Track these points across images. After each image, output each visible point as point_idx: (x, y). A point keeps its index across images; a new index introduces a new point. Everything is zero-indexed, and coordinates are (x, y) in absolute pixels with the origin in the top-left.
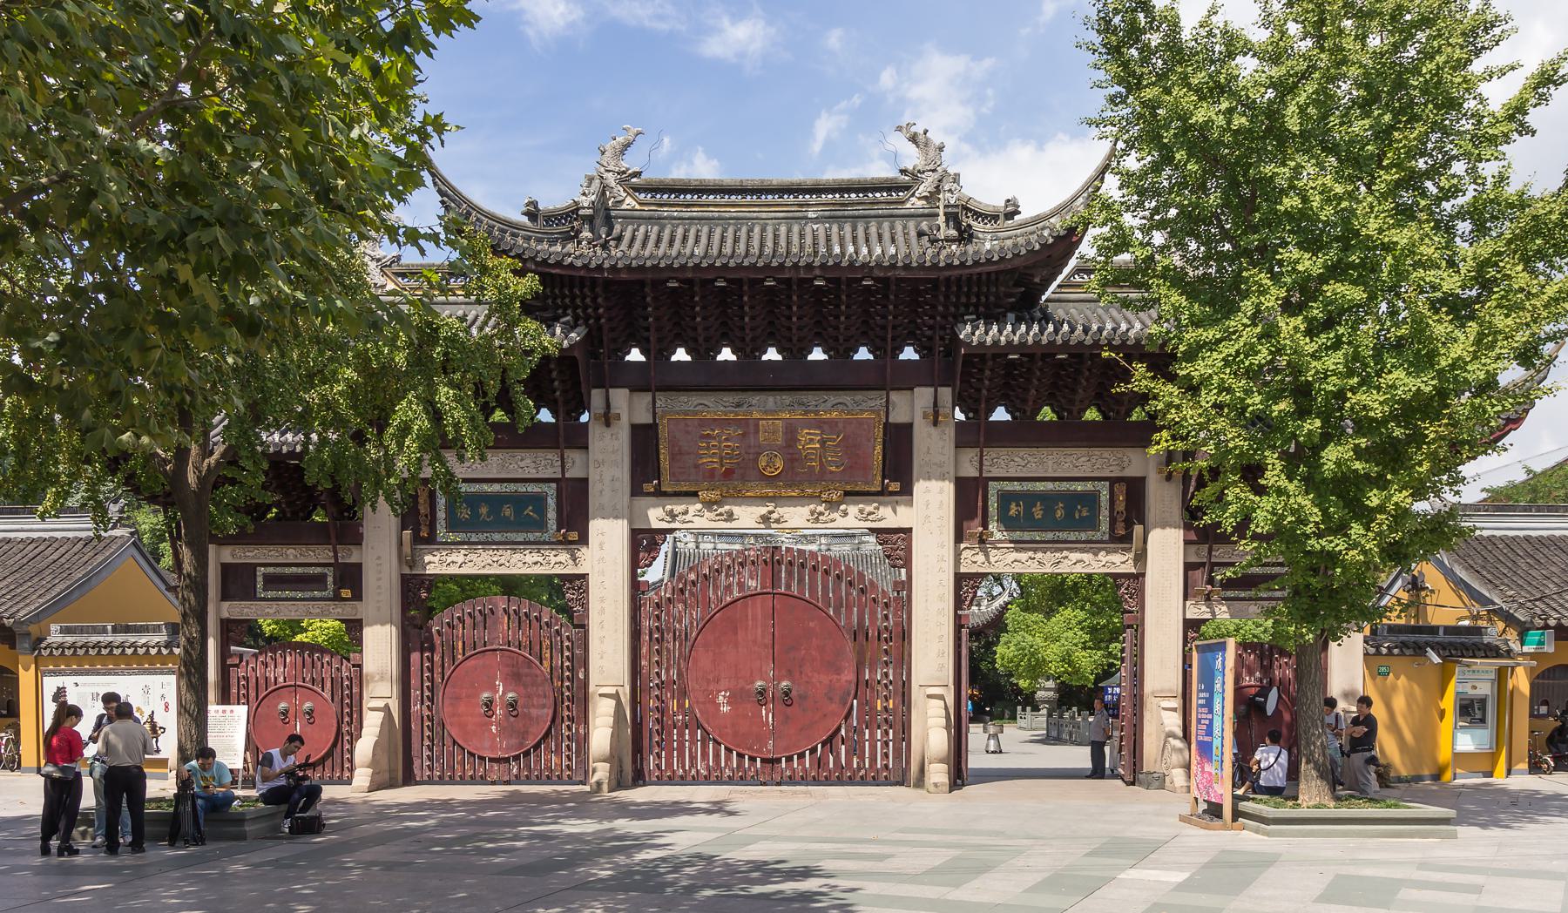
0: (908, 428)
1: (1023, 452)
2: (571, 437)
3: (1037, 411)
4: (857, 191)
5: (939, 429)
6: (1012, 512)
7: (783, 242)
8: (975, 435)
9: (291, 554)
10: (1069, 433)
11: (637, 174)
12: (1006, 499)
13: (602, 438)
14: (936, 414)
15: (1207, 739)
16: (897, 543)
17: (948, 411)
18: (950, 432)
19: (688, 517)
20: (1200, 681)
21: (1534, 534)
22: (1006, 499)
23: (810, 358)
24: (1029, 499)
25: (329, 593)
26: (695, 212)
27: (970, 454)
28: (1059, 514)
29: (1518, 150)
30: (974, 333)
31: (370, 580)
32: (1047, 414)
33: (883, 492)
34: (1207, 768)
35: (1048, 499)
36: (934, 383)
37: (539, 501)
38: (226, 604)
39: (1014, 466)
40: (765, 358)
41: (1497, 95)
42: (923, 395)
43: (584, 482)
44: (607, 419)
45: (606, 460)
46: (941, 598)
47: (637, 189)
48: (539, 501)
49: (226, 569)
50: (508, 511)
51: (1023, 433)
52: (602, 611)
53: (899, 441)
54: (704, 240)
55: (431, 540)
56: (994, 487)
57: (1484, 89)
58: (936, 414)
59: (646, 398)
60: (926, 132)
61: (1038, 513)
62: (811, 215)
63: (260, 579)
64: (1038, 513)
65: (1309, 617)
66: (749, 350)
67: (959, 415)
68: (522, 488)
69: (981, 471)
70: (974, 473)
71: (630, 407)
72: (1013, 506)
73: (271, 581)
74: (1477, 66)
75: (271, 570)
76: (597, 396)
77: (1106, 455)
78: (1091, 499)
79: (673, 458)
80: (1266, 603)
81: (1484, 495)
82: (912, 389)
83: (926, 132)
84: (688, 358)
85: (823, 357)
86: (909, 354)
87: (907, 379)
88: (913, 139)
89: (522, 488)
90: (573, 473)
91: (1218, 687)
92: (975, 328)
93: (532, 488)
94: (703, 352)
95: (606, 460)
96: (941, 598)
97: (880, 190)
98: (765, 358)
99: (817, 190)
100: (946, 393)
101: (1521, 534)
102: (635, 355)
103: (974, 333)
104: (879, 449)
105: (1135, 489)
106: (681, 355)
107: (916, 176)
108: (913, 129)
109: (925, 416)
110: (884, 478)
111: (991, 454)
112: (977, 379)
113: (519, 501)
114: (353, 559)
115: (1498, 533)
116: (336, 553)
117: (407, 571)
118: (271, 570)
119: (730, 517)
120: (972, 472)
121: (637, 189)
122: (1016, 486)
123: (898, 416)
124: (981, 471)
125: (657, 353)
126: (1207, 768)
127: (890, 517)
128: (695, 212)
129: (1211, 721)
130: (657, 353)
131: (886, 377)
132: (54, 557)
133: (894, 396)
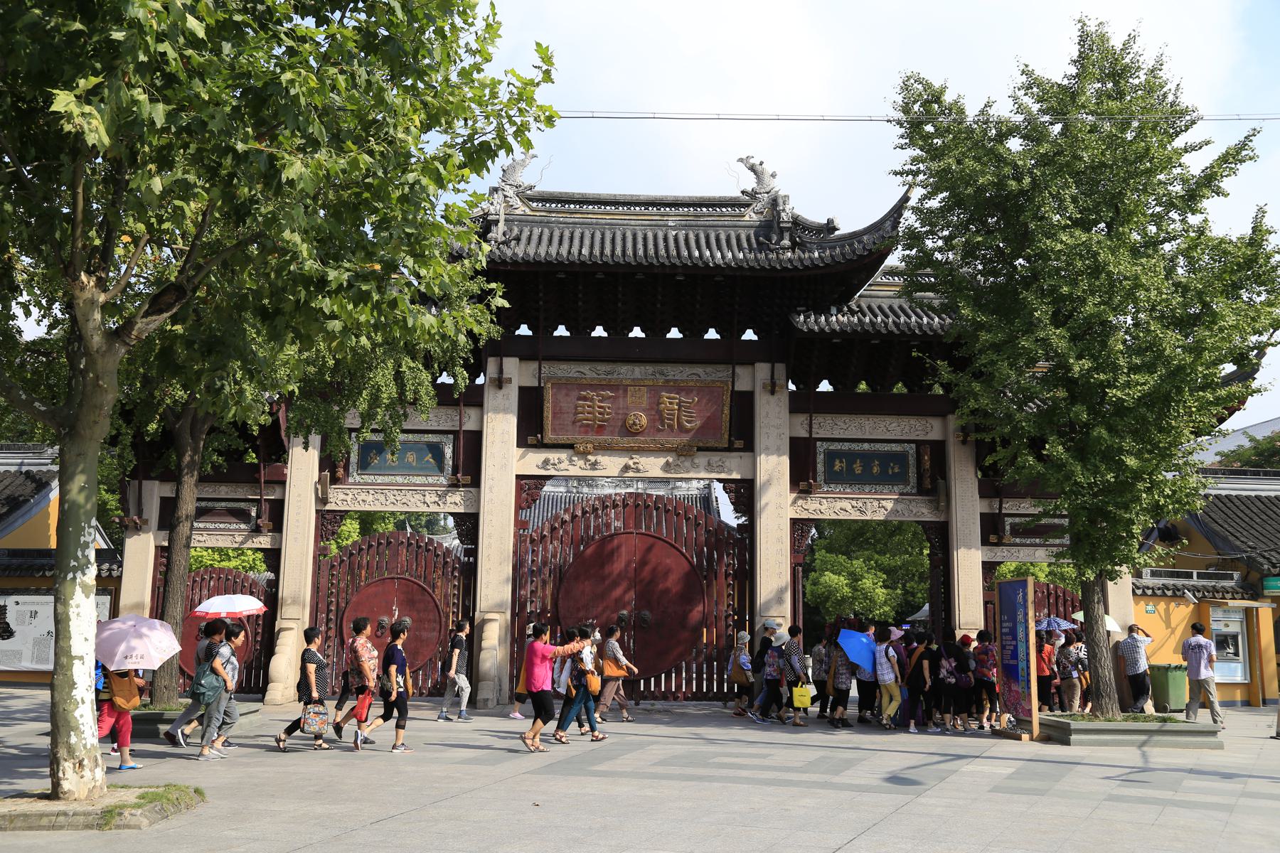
1: (846, 418)
3: (856, 385)
4: (707, 206)
5: (776, 397)
6: (837, 468)
7: (651, 246)
8: (804, 403)
10: (878, 405)
11: (531, 188)
12: (831, 456)
14: (773, 384)
15: (1013, 662)
16: (745, 495)
17: (783, 382)
18: (785, 400)
19: (562, 466)
21: (1263, 494)
22: (831, 456)
23: (668, 336)
24: (850, 457)
26: (577, 218)
27: (802, 419)
28: (875, 470)
29: (1211, 205)
30: (806, 321)
32: (899, 388)
33: (730, 449)
34: (1014, 687)
35: (867, 457)
36: (771, 360)
39: (834, 427)
40: (631, 335)
41: (1196, 164)
42: (763, 370)
46: (779, 540)
47: (531, 199)
51: (840, 404)
53: (743, 408)
54: (587, 242)
56: (821, 447)
57: (1186, 159)
58: (773, 384)
59: (534, 366)
60: (761, 164)
61: (858, 469)
62: (671, 224)
63: (1008, 528)
64: (858, 469)
65: (1091, 560)
66: (618, 329)
67: (792, 387)
68: (855, 446)
69: (810, 432)
71: (518, 372)
72: (837, 462)
73: (1016, 531)
74: (1179, 142)
75: (1017, 520)
77: (912, 422)
78: (901, 458)
79: (554, 414)
80: (1055, 549)
81: (1218, 458)
82: (753, 364)
83: (761, 164)
84: (568, 334)
87: (749, 355)
88: (752, 169)
89: (855, 446)
90: (470, 425)
91: (1020, 617)
92: (807, 317)
93: (896, 448)
94: (580, 329)
96: (779, 540)
97: (726, 206)
98: (631, 335)
99: (676, 204)
100: (780, 369)
101: (1253, 494)
103: (806, 321)
104: (727, 411)
105: (938, 450)
106: (561, 331)
107: (753, 195)
108: (752, 161)
109: (764, 387)
110: (730, 436)
111: (818, 419)
112: (802, 358)
115: (1234, 493)
118: (1017, 520)
119: (594, 465)
121: (531, 199)
123: (742, 385)
124: (810, 432)
126: (1014, 687)
128: (577, 218)
129: (1016, 647)
131: (731, 353)
132: (1247, 519)
133: (739, 370)
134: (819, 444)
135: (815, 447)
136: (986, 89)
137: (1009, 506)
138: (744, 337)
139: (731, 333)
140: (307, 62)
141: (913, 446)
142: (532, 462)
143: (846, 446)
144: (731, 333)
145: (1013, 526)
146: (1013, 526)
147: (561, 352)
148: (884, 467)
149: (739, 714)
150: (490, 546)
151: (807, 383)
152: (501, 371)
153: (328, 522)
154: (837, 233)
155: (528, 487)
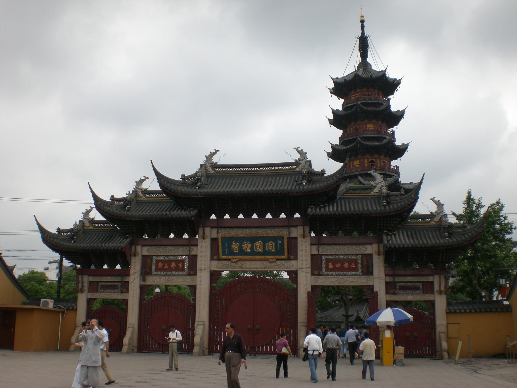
0: (296, 238)
2: (192, 243)
8: (317, 242)
9: (409, 279)
12: (328, 261)
13: (202, 242)
14: (304, 235)
16: (293, 275)
20: (106, 302)
25: (285, 256)
27: (314, 247)
31: (131, 286)
36: (304, 225)
37: (183, 261)
38: (90, 294)
43: (196, 256)
44: (204, 237)
45: (203, 250)
48: (356, 261)
49: (91, 283)
50: (173, 265)
52: (200, 293)
53: (293, 242)
55: (150, 273)
59: (215, 231)
70: (316, 253)
71: (211, 233)
73: (103, 287)
75: (401, 284)
76: (201, 230)
85: (299, 216)
86: (297, 215)
90: (193, 253)
93: (353, 257)
95: (203, 250)
100: (307, 228)
102: (213, 217)
111: (321, 248)
113: (350, 262)
114: (127, 280)
116: (394, 279)
117: (143, 283)
120: (316, 252)
122: (330, 257)
123: (293, 235)
125: (220, 216)
127: (293, 265)
130: (220, 216)
131: (290, 223)
134: (323, 256)
135: (322, 258)
136: (444, 206)
137: (397, 279)
138: (295, 216)
139: (290, 215)
140: (448, 279)
141: (360, 256)
142: (215, 265)
143: (334, 257)
144: (290, 215)
145: (399, 286)
146: (399, 286)
147: (227, 226)
148: (350, 265)
149: (169, 370)
150: (200, 297)
151: (318, 234)
152: (204, 233)
153: (144, 289)
154: (325, 175)
155: (215, 275)
